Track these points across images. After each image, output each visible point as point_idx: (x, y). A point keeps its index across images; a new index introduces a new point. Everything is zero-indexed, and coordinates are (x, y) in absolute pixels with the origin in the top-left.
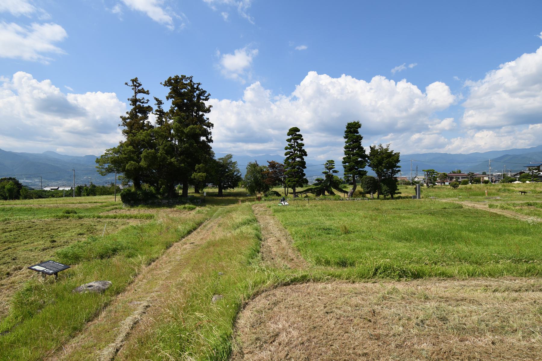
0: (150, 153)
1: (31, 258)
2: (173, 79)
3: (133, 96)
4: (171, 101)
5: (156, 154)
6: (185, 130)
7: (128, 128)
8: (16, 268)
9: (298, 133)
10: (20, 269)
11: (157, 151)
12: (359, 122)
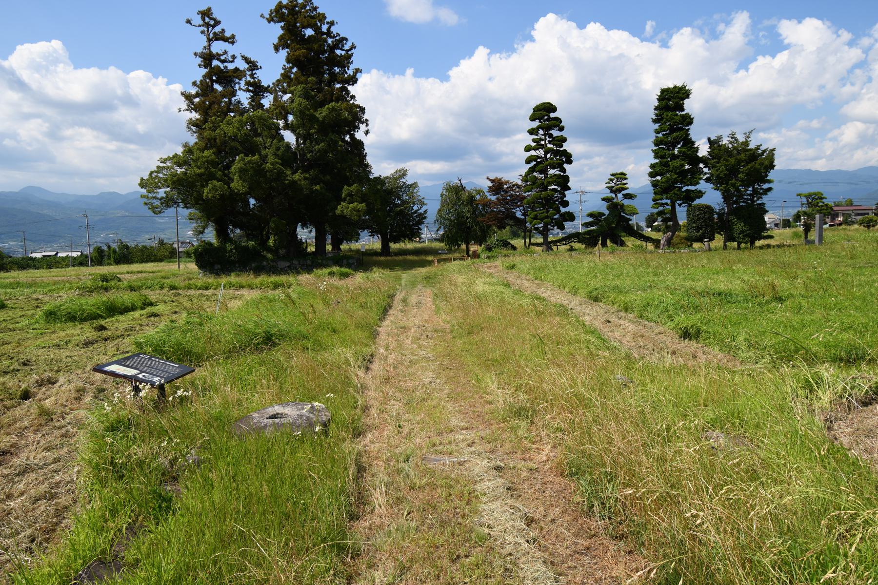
0: (249, 162)
1: (64, 360)
2: (286, 7)
3: (205, 47)
4: (284, 53)
5: (262, 164)
6: (317, 115)
7: (200, 114)
8: (42, 380)
9: (552, 115)
10: (53, 383)
11: (264, 158)
12: (685, 87)
